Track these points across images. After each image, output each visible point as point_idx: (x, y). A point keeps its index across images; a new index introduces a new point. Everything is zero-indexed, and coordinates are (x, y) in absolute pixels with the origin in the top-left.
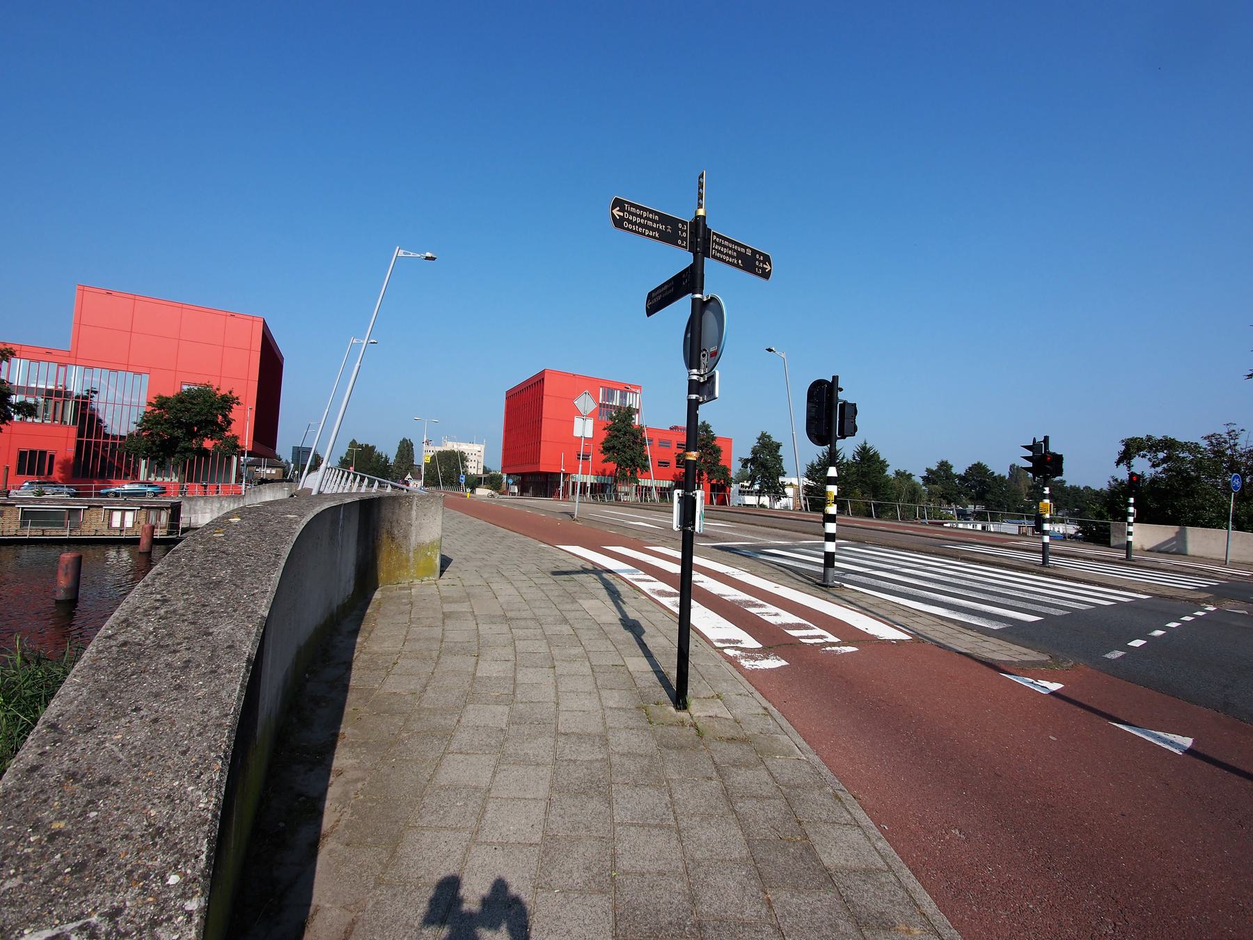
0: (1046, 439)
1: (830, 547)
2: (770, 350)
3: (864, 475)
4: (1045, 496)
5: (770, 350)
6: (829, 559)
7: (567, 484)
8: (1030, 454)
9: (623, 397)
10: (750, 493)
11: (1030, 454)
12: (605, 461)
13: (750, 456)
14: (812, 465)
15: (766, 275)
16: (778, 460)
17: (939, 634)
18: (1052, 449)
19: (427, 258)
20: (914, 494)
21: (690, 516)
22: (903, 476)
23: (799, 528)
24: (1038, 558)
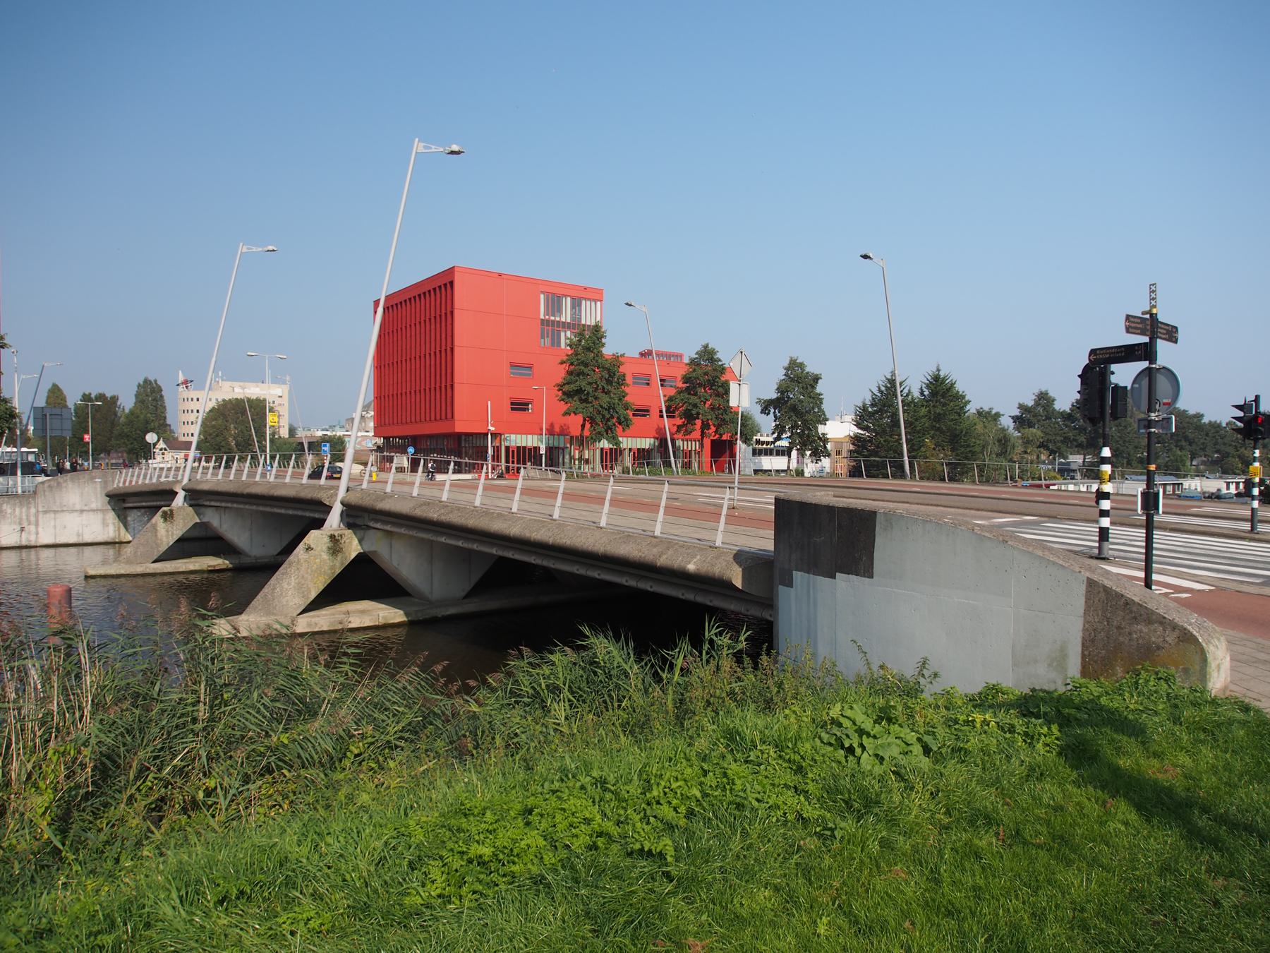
0: (1257, 399)
1: (1105, 522)
2: (866, 257)
3: (938, 418)
4: (1255, 459)
5: (866, 257)
6: (1104, 534)
7: (497, 450)
8: (1241, 414)
9: (576, 304)
10: (768, 453)
11: (1241, 414)
12: (567, 414)
13: (774, 396)
14: (864, 408)
15: (1176, 342)
16: (817, 400)
17: (1223, 585)
18: (1262, 409)
19: (452, 153)
20: (1004, 441)
21: (1152, 503)
22: (990, 417)
23: (995, 508)
24: (1246, 526)
